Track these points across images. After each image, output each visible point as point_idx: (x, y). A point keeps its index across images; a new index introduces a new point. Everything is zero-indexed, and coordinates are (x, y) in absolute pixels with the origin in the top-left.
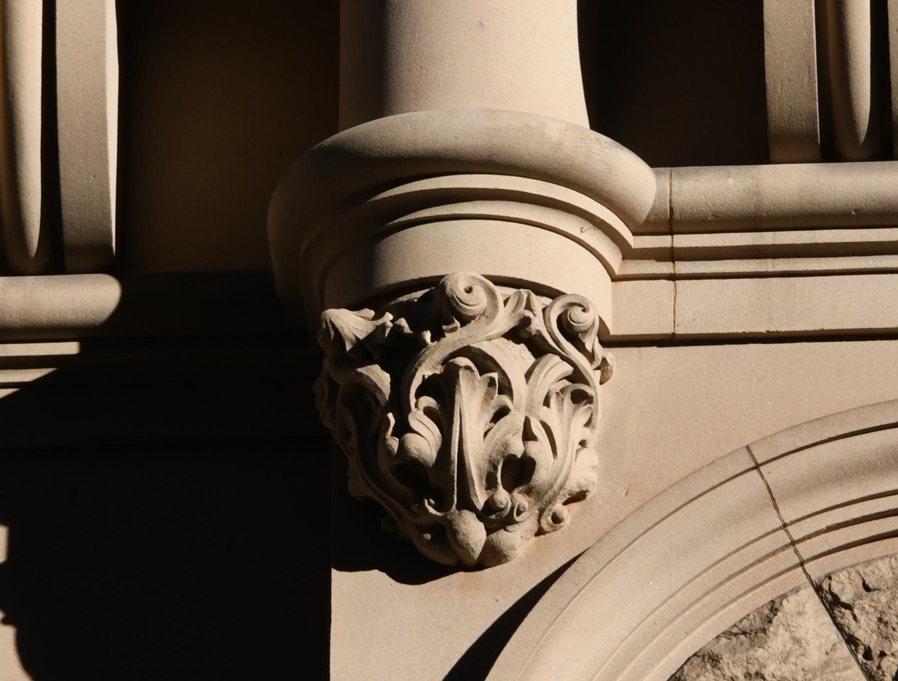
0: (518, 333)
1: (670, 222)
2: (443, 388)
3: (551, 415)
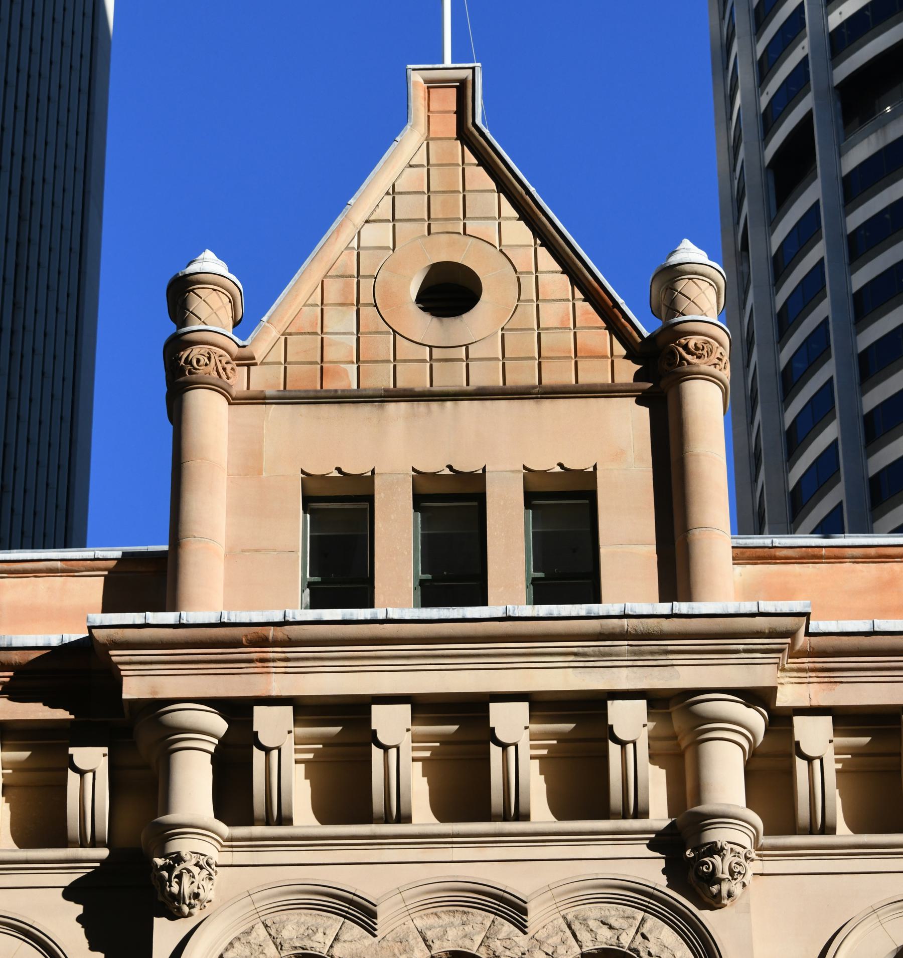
0: (197, 865)
1: (232, 839)
2: (179, 877)
3: (204, 883)
